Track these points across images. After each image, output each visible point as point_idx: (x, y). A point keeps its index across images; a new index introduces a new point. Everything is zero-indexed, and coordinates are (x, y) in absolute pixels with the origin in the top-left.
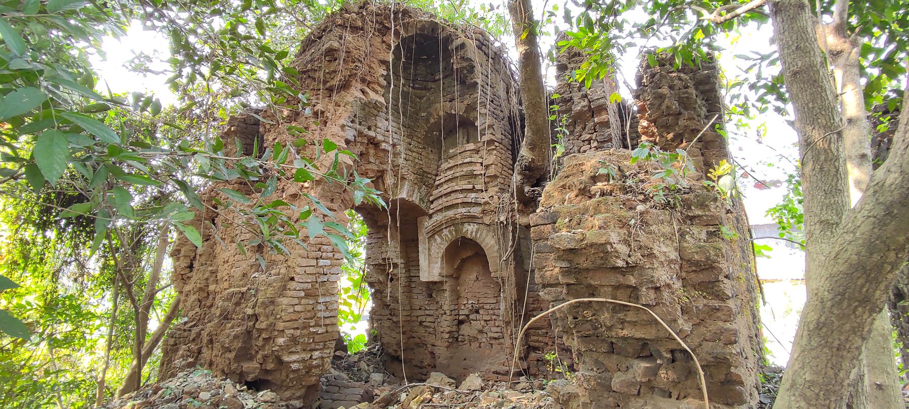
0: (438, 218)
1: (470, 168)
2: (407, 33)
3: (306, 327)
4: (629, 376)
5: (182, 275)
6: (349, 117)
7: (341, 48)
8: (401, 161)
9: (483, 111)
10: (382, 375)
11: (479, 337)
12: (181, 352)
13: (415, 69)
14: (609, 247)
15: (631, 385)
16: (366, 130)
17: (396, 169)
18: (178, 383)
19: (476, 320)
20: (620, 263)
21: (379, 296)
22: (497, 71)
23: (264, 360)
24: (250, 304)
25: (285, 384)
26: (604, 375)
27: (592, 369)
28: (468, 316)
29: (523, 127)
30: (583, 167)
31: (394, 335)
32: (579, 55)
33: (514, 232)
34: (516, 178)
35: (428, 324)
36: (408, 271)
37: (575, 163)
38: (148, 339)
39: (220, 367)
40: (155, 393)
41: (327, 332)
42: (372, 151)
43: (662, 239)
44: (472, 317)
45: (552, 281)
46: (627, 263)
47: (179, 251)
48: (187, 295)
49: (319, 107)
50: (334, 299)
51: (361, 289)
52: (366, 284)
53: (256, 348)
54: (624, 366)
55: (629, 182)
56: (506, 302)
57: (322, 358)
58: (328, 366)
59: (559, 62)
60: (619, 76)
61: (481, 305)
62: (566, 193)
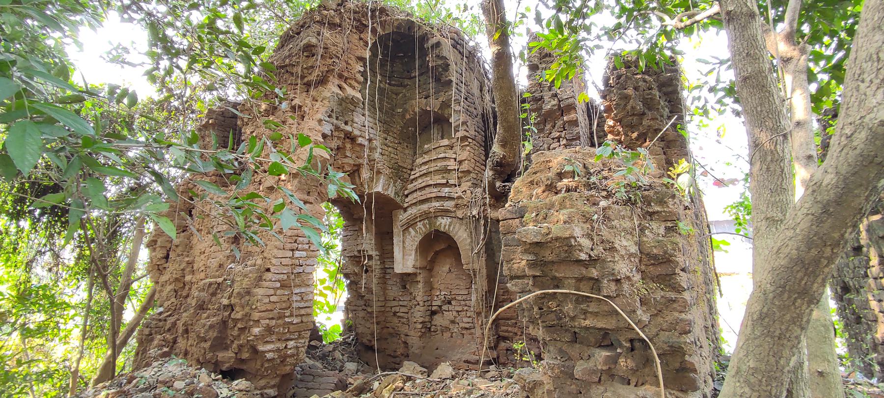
1: (444, 163)
2: (384, 30)
3: (281, 317)
4: (591, 364)
6: (327, 112)
7: (319, 44)
8: (377, 155)
9: (457, 108)
10: (356, 364)
11: (451, 327)
12: (156, 342)
13: (392, 66)
14: (573, 241)
16: (343, 125)
17: (372, 163)
20: (583, 256)
24: (226, 295)
26: (567, 363)
27: (556, 358)
28: (440, 307)
32: (550, 55)
33: (485, 226)
34: (488, 174)
36: (383, 263)
37: (542, 160)
38: (123, 329)
39: (196, 356)
40: (129, 382)
41: (302, 322)
43: (623, 234)
44: (445, 307)
45: (519, 273)
46: (590, 256)
47: (155, 242)
49: (297, 102)
50: (309, 289)
51: (337, 281)
54: (586, 355)
55: (593, 179)
56: (477, 293)
57: (297, 348)
58: (303, 355)
60: (587, 76)
61: (453, 296)
62: (534, 189)
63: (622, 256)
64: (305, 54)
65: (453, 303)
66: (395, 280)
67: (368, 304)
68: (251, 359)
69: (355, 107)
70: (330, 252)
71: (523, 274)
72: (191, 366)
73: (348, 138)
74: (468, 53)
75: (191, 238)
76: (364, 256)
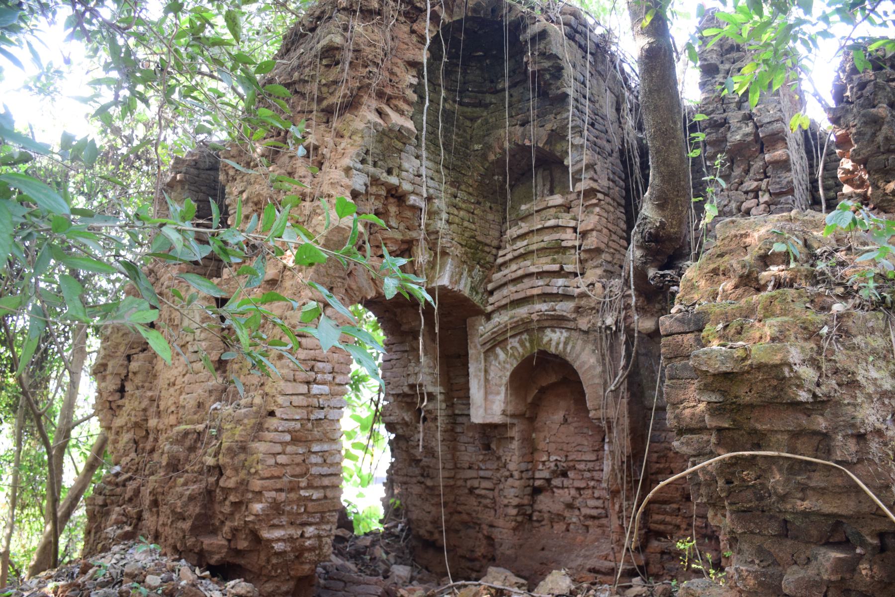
0: (502, 319)
1: (556, 236)
2: (451, 15)
3: (294, 488)
4: (811, 572)
5: (110, 402)
6: (358, 155)
7: (346, 44)
8: (441, 225)
9: (578, 141)
10: (408, 568)
11: (567, 514)
12: (114, 517)
13: (464, 73)
14: (786, 370)
15: (813, 586)
16: (385, 174)
17: (433, 237)
18: (114, 561)
19: (563, 488)
20: (803, 396)
21: (403, 444)
22: (600, 74)
23: (234, 535)
24: (211, 450)
25: (264, 572)
26: (771, 570)
27: (752, 562)
28: (548, 481)
29: (645, 167)
30: (748, 240)
31: (427, 507)
32: (738, 48)
33: (629, 343)
34: (634, 254)
35: (483, 492)
36: (450, 405)
37: (733, 232)
38: (63, 496)
39: (171, 541)
40: (84, 571)
41: (325, 497)
42: (393, 209)
43: (871, 358)
44: (556, 482)
45: (694, 424)
46: (815, 395)
47: (104, 366)
48: (117, 433)
49: (311, 140)
50: (334, 447)
51: (373, 434)
52: (383, 426)
53: (220, 516)
54: (803, 556)
55: (821, 266)
56: (613, 459)
57: (319, 537)
58: (328, 549)
59: (705, 60)
60: (805, 85)
61: (571, 464)
62: (719, 283)
63: (869, 396)
64: (324, 62)
65: (571, 474)
66: (471, 434)
67: (427, 472)
68: (251, 551)
69: (405, 144)
70: (361, 387)
71: (702, 425)
72: (165, 555)
73: (392, 196)
74: (594, 46)
75: (155, 361)
76: (422, 394)
